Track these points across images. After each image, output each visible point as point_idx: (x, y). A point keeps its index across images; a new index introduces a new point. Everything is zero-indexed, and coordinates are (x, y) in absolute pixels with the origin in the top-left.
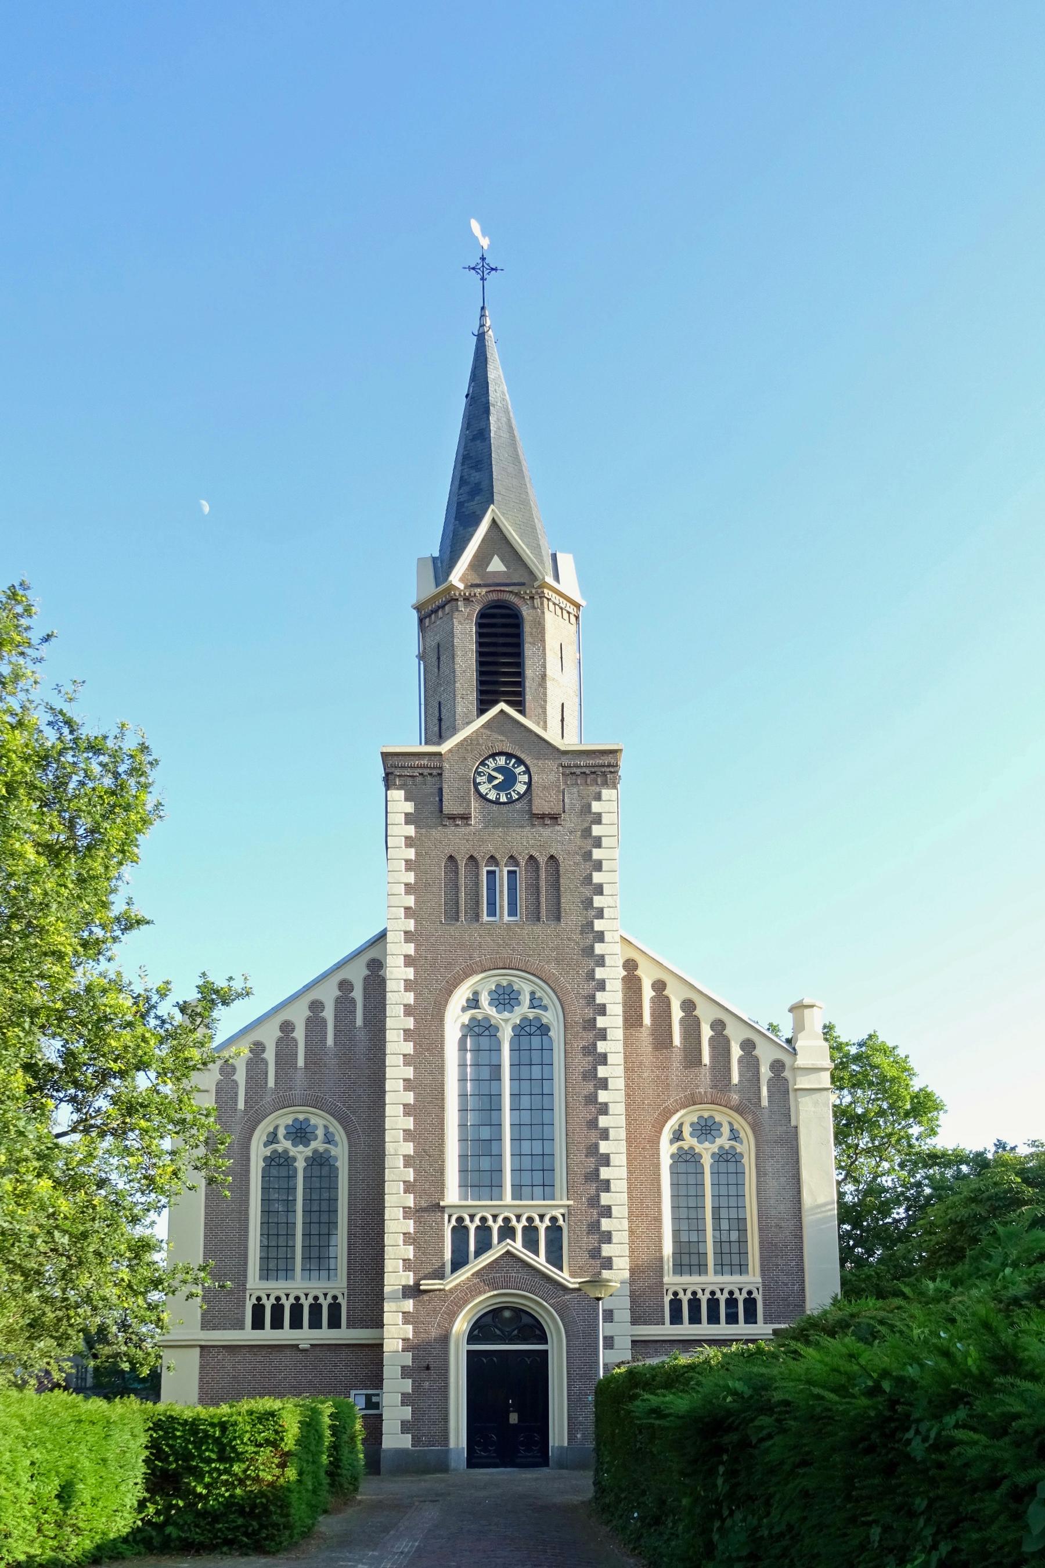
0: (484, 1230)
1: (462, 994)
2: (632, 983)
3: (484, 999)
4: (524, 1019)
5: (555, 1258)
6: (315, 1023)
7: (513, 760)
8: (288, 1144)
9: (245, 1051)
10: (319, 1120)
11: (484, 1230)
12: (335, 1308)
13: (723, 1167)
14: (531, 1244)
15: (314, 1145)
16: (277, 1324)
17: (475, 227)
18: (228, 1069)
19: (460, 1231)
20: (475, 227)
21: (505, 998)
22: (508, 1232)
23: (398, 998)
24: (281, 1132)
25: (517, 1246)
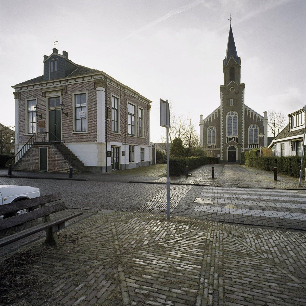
0: (230, 139)
3: (230, 114)
10: (214, 127)
11: (230, 139)
14: (235, 140)
19: (228, 139)
21: (232, 114)
22: (232, 139)
23: (222, 115)
25: (233, 140)
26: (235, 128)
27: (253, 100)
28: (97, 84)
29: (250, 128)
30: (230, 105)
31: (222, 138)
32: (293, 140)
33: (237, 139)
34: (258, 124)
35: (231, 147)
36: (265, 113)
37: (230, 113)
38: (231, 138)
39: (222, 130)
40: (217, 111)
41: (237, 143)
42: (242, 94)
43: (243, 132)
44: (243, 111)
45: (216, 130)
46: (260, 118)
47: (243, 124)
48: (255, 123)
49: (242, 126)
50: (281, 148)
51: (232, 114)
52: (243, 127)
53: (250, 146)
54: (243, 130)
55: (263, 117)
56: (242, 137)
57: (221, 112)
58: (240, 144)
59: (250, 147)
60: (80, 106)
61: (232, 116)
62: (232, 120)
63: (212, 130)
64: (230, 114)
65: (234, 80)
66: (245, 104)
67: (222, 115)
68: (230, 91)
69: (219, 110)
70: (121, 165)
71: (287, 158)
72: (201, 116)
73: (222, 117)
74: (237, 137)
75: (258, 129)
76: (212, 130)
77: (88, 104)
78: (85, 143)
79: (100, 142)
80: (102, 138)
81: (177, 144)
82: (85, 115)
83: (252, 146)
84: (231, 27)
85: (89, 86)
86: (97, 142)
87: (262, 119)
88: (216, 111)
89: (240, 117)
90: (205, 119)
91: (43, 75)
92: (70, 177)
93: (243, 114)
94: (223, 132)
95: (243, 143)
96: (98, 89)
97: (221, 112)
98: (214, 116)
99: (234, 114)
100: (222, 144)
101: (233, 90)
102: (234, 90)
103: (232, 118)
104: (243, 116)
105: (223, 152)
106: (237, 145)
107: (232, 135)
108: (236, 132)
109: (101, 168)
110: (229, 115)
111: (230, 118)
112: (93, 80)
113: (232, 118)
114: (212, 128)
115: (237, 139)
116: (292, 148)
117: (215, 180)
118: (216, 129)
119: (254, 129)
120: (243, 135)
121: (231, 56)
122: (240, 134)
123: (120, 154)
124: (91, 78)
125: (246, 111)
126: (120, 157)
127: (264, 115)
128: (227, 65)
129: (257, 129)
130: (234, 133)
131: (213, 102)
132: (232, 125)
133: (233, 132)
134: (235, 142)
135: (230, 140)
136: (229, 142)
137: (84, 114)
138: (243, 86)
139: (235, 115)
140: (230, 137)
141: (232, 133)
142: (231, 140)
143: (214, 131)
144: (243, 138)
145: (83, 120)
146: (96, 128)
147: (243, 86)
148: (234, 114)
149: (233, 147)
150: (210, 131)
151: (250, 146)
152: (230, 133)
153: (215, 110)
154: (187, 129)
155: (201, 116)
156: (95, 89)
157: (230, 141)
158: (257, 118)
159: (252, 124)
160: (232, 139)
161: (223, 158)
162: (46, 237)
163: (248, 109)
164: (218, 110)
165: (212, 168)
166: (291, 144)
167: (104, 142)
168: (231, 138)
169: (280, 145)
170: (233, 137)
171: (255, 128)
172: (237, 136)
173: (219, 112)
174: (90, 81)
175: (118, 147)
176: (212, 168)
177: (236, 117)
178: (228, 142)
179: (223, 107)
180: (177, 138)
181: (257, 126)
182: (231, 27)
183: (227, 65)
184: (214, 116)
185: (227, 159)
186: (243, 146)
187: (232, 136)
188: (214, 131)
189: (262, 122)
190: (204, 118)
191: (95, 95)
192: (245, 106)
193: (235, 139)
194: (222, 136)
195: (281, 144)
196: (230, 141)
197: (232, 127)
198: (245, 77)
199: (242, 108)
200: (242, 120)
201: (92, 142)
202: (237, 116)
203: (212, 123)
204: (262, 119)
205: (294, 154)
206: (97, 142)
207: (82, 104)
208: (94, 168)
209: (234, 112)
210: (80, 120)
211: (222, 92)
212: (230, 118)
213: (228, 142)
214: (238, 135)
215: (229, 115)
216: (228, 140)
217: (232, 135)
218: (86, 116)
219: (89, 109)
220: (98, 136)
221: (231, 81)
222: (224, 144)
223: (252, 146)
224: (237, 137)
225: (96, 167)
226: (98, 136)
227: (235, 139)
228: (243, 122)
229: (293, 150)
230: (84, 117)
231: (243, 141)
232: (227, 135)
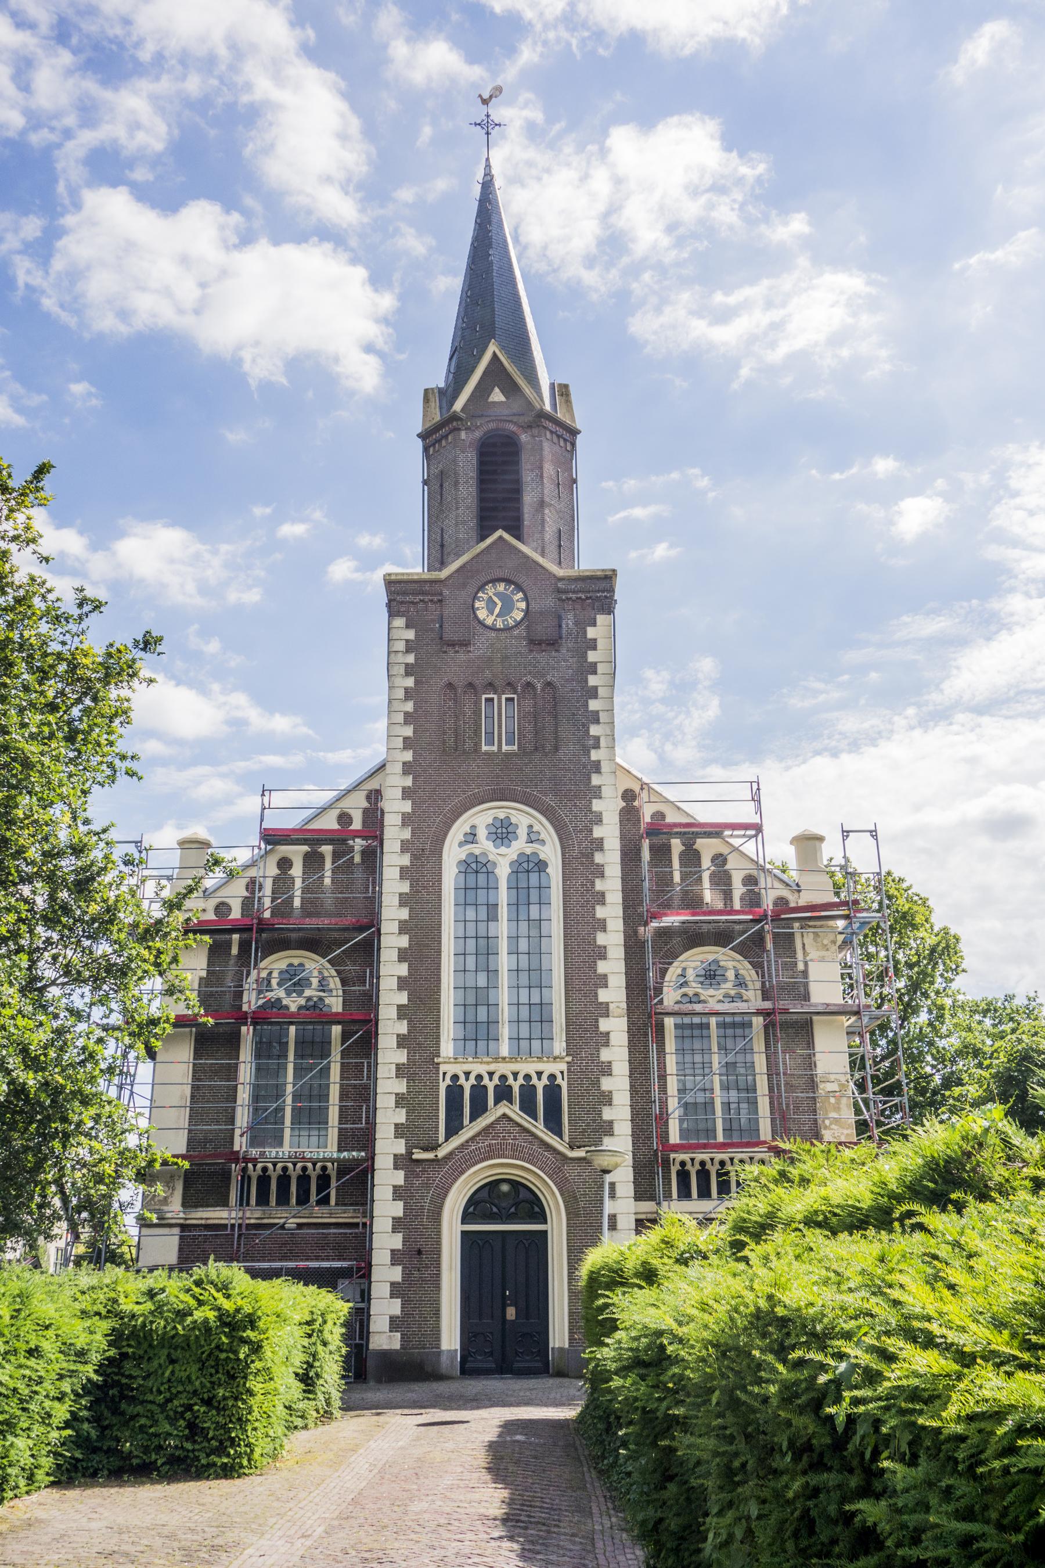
0: (479, 1091)
3: (482, 833)
11: (479, 1091)
19: (454, 1093)
21: (503, 833)
22: (504, 1093)
30: (477, 745)
33: (553, 1092)
35: (493, 1186)
37: (481, 818)
38: (491, 1086)
49: (602, 953)
51: (503, 833)
57: (395, 807)
61: (503, 861)
62: (503, 896)
64: (482, 833)
65: (516, 529)
68: (482, 614)
89: (581, 861)
91: (713, 126)
97: (395, 807)
99: (522, 832)
100: (388, 1145)
102: (518, 615)
103: (503, 872)
106: (558, 1166)
108: (540, 1014)
110: (471, 837)
111: (476, 869)
113: (503, 872)
115: (553, 1092)
121: (492, 348)
122: (584, 1034)
125: (629, 814)
130: (524, 1029)
132: (503, 946)
135: (479, 1108)
140: (482, 1069)
141: (505, 1031)
142: (496, 1112)
147: (598, 592)
148: (522, 832)
149: (515, 1184)
152: (478, 1032)
157: (483, 1122)
161: (395, 1323)
162: (123, 329)
168: (491, 1086)
172: (552, 1065)
177: (541, 866)
185: (450, 1338)
187: (506, 1061)
197: (504, 962)
199: (595, 780)
200: (606, 1070)
202: (551, 852)
209: (523, 817)
211: (399, 622)
212: (476, 869)
214: (559, 1046)
215: (471, 837)
216: (464, 1102)
222: (418, 1155)
232: (447, 1048)
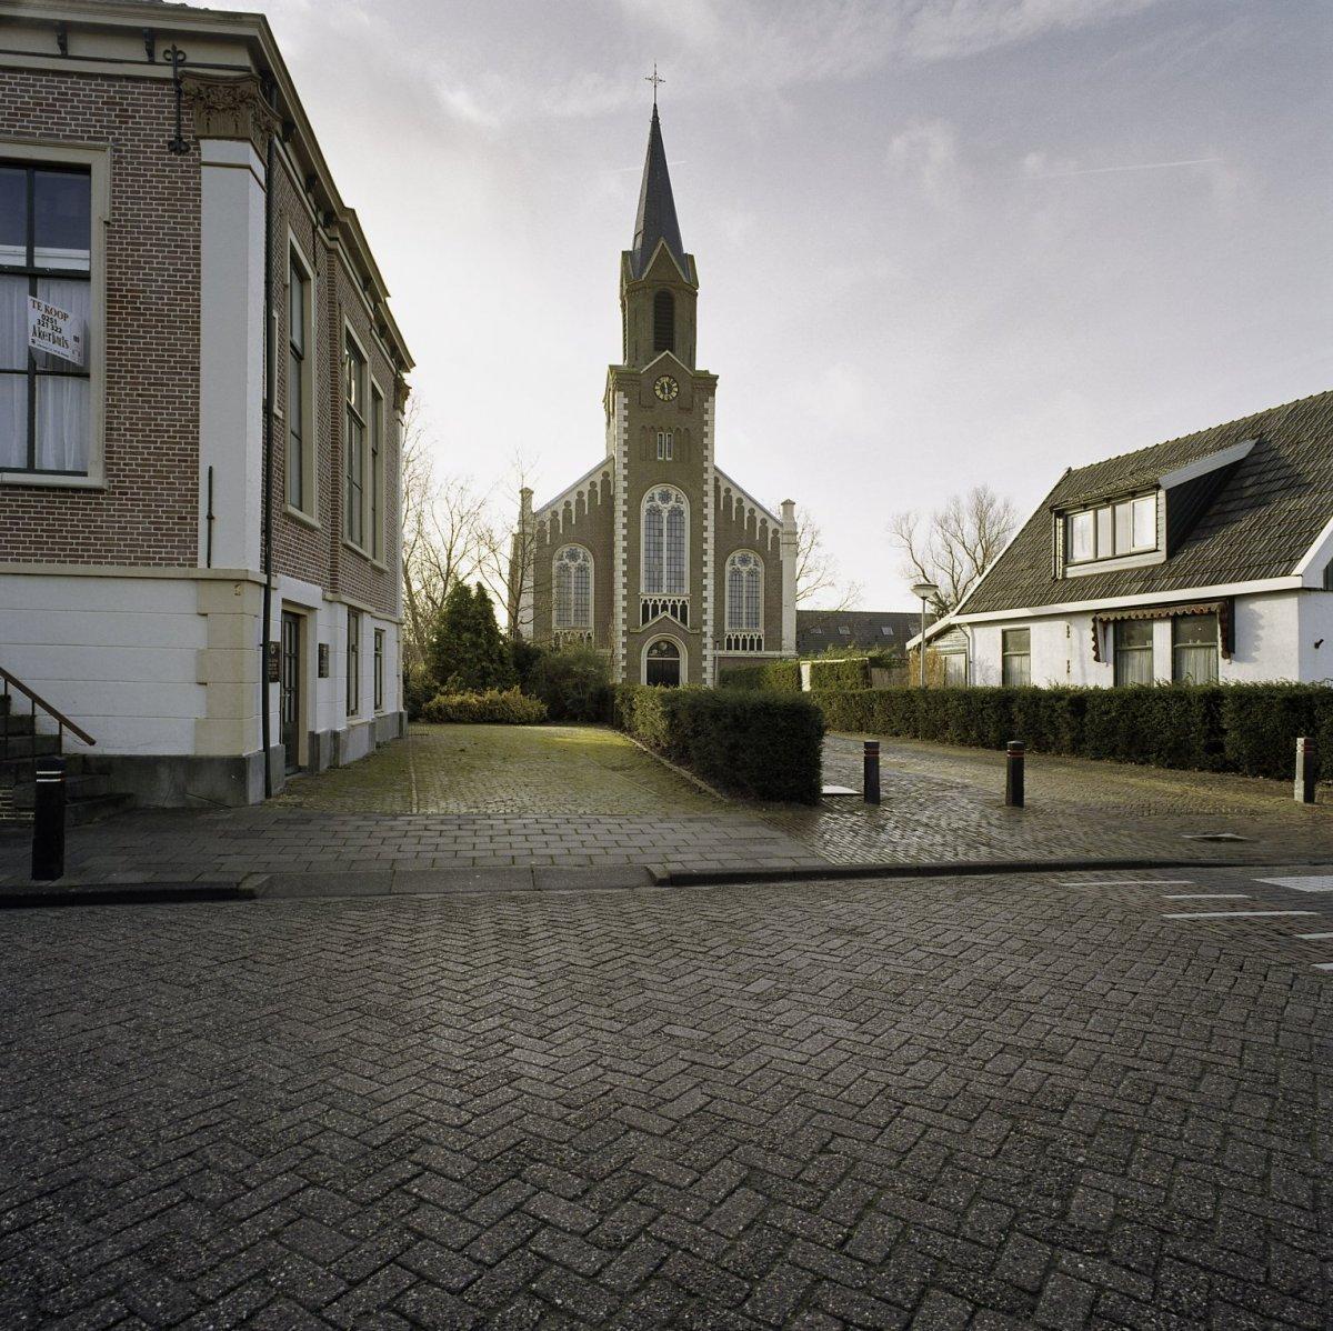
0: (655, 607)
1: (647, 495)
2: (717, 488)
3: (657, 497)
4: (673, 507)
5: (684, 620)
6: (580, 502)
7: (1162, 633)
8: (567, 561)
9: (549, 514)
10: (581, 550)
11: (655, 607)
12: (759, 641)
13: (751, 578)
14: (674, 613)
15: (579, 561)
16: (759, 648)
17: (1300, 741)
18: (542, 524)
19: (646, 607)
20: (1300, 741)
21: (665, 497)
22: (665, 608)
23: (621, 496)
24: (565, 555)
25: (668, 614)
26: (675, 560)
27: (746, 450)
28: (210, 108)
29: (733, 563)
30: (656, 457)
31: (620, 604)
32: (1104, 616)
34: (760, 548)
36: (788, 504)
37: (656, 490)
39: (620, 568)
40: (598, 479)
41: (682, 626)
42: (706, 417)
43: (709, 582)
44: (709, 488)
45: (591, 565)
46: (771, 526)
47: (709, 547)
48: (751, 547)
50: (1005, 649)
51: (665, 497)
52: (709, 558)
53: (729, 640)
54: (709, 569)
55: (781, 525)
56: (705, 599)
58: (695, 632)
59: (729, 648)
60: (22, 262)
61: (665, 508)
63: (573, 565)
64: (657, 497)
66: (717, 463)
67: (621, 496)
68: (658, 393)
69: (606, 474)
70: (314, 737)
71: (1036, 696)
72: (526, 494)
73: (620, 508)
74: (685, 599)
75: (761, 569)
76: (573, 565)
77: (110, 258)
78: (80, 569)
79: (222, 563)
80: (237, 540)
81: (473, 617)
82: (71, 342)
83: (737, 640)
84: (655, 110)
85: (124, 117)
86: (202, 563)
87: (776, 532)
88: (592, 479)
89: (698, 515)
90: (543, 510)
92: (36, 876)
93: (710, 500)
94: (705, 564)
95: (709, 629)
96: (211, 150)
98: (586, 498)
99: (674, 498)
100: (620, 627)
101: (670, 391)
103: (665, 515)
104: (710, 511)
105: (624, 664)
106: (686, 637)
107: (665, 592)
109: (238, 766)
112: (167, 72)
113: (665, 515)
114: (573, 556)
115: (684, 608)
116: (1096, 648)
117: (1029, 821)
118: (591, 559)
119: (745, 569)
120: (709, 593)
121: (662, 241)
122: (697, 587)
123: (310, 665)
124: (151, 53)
126: (309, 686)
127: (785, 512)
128: (644, 275)
129: (759, 569)
131: (574, 443)
133: (669, 579)
134: (677, 621)
135: (655, 613)
136: (652, 622)
137: (69, 329)
138: (708, 383)
139: (676, 505)
140: (656, 598)
142: (662, 615)
143: (582, 569)
144: (709, 605)
145: (49, 388)
146: (190, 459)
148: (674, 498)
150: (565, 568)
151: (729, 640)
152: (655, 584)
153: (590, 474)
154: (1309, 470)
155: (526, 494)
156: (178, 146)
157: (657, 619)
158: (759, 524)
159: (740, 547)
160: (665, 608)
163: (723, 485)
164: (604, 476)
165: (867, 745)
166: (1094, 629)
167: (253, 565)
169: (1000, 635)
170: (666, 598)
171: (751, 566)
173: (607, 483)
174: (129, 78)
175: (297, 616)
176: (867, 745)
178: (645, 620)
179: (626, 460)
180: (467, 590)
181: (759, 558)
182: (655, 110)
183: (644, 275)
184: (586, 498)
186: (709, 641)
187: (663, 595)
188: (582, 569)
189: (776, 541)
190: (537, 503)
191: (191, 195)
192: (716, 469)
193: (674, 607)
194: (620, 591)
195: (1004, 633)
196: (657, 619)
198: (718, 340)
201: (146, 560)
202: (686, 507)
203: (562, 536)
204: (776, 532)
205: (1101, 677)
206: (202, 563)
207: (36, 250)
208: (164, 773)
209: (674, 492)
210: (20, 384)
213: (645, 620)
214: (687, 590)
216: (649, 611)
217: (665, 592)
218: (86, 354)
219: (116, 299)
220: (210, 518)
221: (659, 348)
223: (737, 640)
224: (683, 599)
225: (190, 766)
226: (210, 518)
227: (674, 607)
228: (710, 535)
229: (1097, 659)
230: (70, 354)
231: (709, 617)
232: (643, 590)
